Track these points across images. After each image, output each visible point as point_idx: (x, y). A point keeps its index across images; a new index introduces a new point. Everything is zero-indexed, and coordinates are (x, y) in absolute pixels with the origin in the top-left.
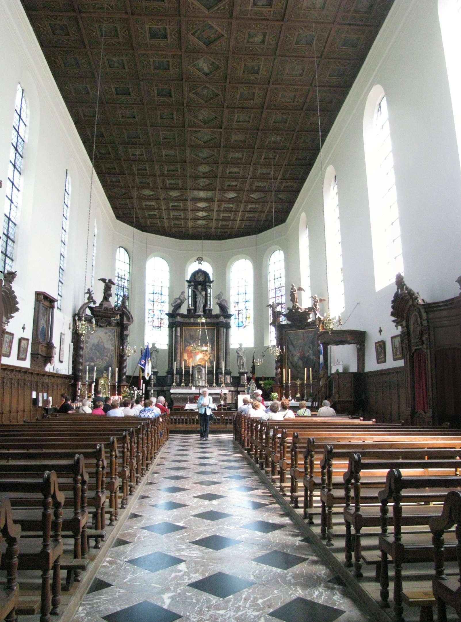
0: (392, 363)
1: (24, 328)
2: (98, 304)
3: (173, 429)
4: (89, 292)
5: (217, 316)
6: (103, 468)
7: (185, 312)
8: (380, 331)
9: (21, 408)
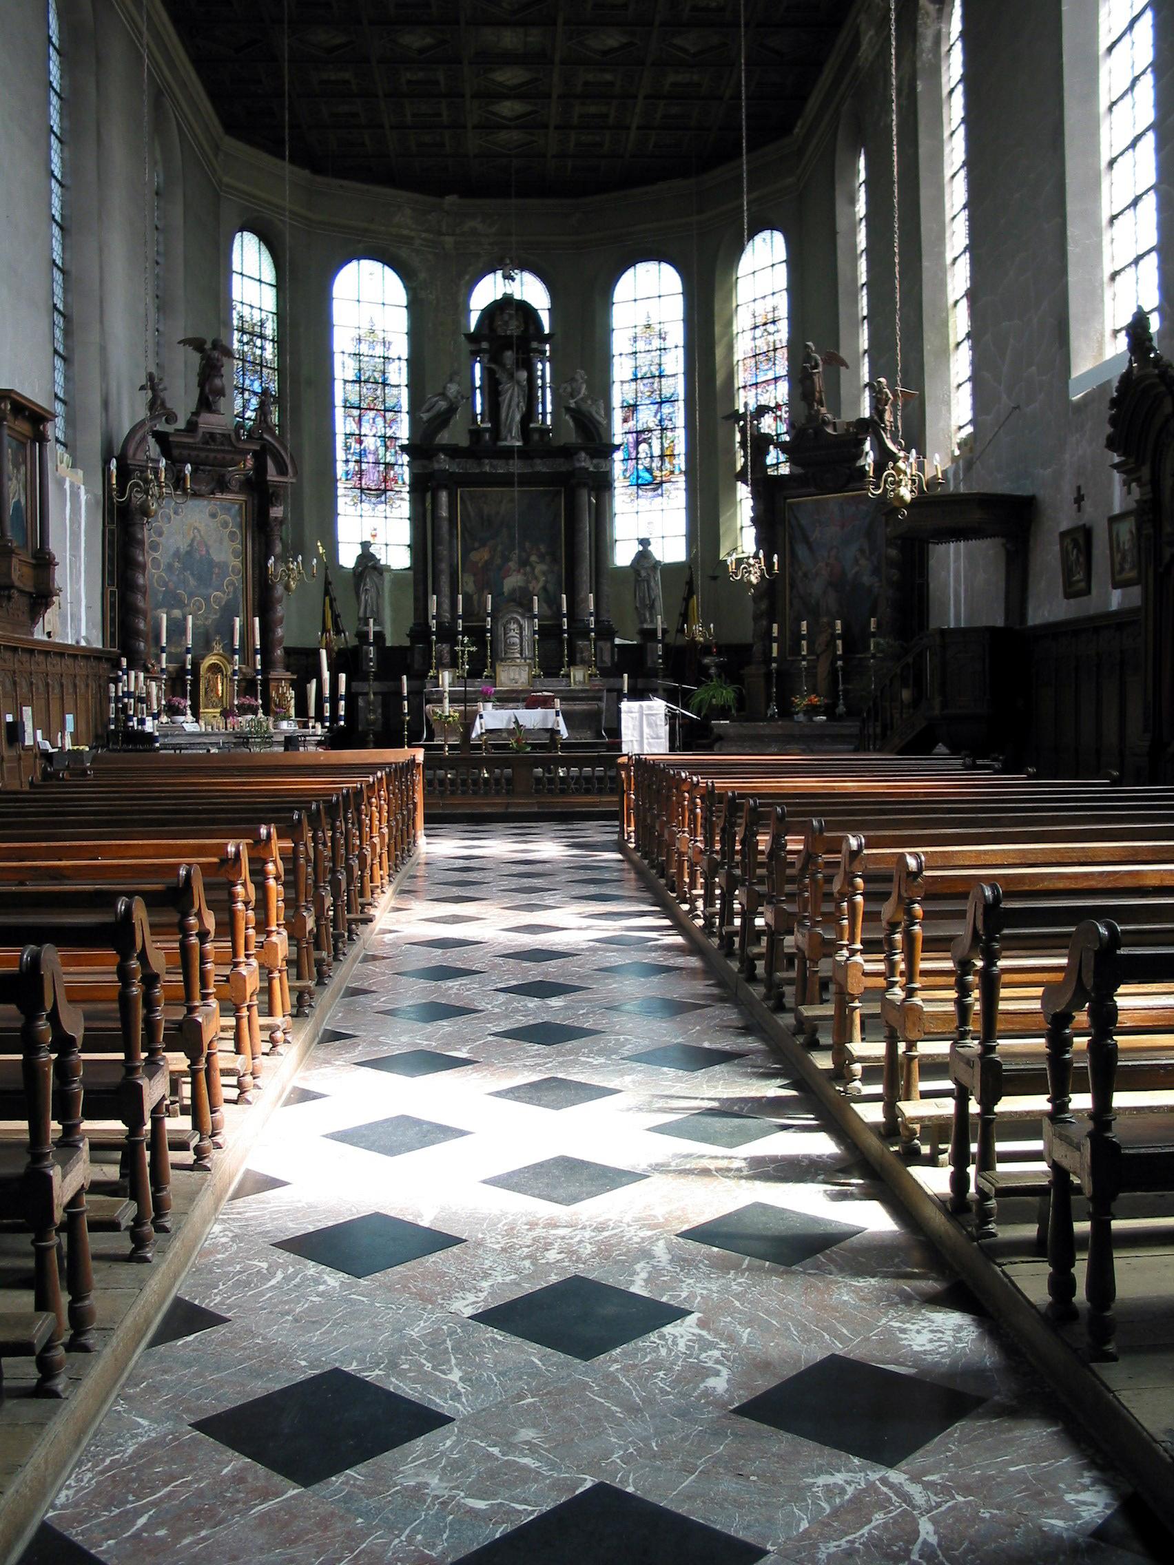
7: (464, 441)
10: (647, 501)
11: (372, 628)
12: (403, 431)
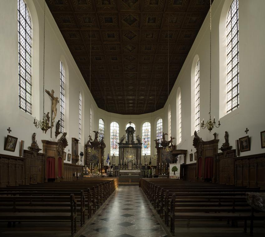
0: (194, 161)
1: (69, 151)
2: (93, 141)
3: (120, 184)
4: (90, 136)
5: (137, 144)
6: (99, 190)
7: (125, 143)
8: (192, 150)
9: (70, 177)
10: (146, 149)
11: (114, 164)
12: (118, 141)
